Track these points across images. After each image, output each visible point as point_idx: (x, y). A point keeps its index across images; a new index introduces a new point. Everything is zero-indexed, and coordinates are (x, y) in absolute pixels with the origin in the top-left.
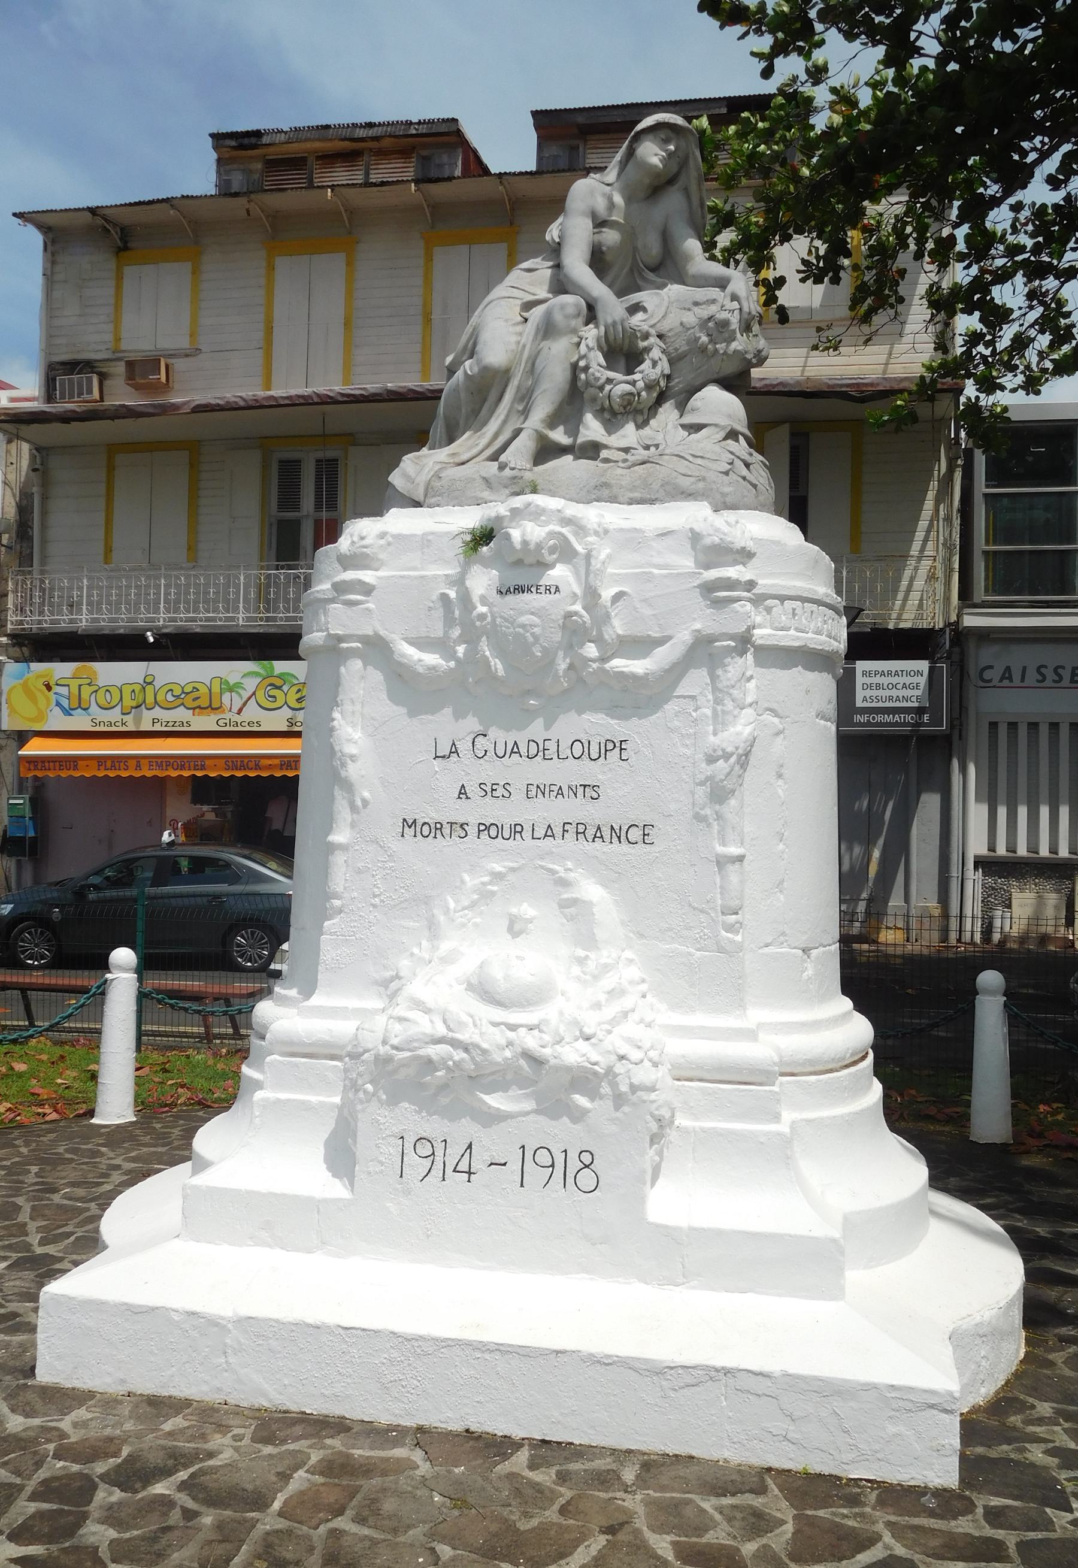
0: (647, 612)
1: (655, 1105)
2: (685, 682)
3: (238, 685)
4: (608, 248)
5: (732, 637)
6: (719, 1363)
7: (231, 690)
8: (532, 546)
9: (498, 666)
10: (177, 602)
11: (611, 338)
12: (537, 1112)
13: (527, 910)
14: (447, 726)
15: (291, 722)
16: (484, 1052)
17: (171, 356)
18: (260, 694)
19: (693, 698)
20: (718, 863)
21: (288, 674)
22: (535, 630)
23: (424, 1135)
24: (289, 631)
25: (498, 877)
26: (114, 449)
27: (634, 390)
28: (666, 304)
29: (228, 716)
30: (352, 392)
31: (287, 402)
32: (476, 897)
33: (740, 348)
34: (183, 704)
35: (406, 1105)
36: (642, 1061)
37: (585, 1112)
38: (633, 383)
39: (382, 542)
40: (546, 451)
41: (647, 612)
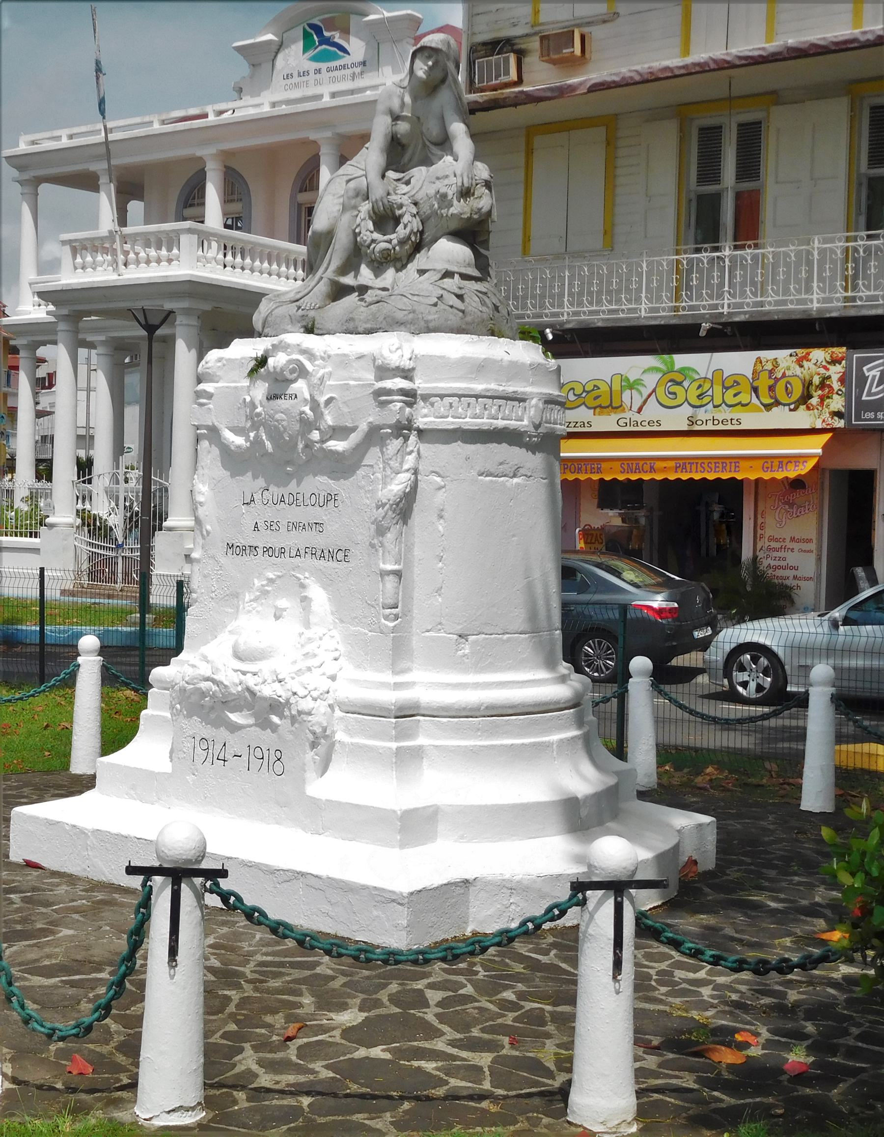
0: (346, 410)
1: (310, 724)
2: (368, 455)
3: (638, 382)
4: (402, 135)
5: (389, 427)
6: (298, 869)
7: (631, 388)
8: (278, 370)
9: (268, 445)
10: (581, 294)
11: (377, 211)
12: (255, 725)
13: (283, 603)
14: (250, 483)
15: (692, 421)
16: (226, 686)
17: (589, 24)
18: (660, 391)
19: (372, 466)
20: (381, 574)
21: (689, 369)
22: (284, 423)
23: (204, 736)
24: (690, 322)
25: (271, 581)
26: (532, 131)
27: (390, 246)
28: (423, 178)
29: (628, 415)
30: (750, 54)
31: (682, 71)
32: (258, 594)
33: (455, 212)
34: (584, 403)
35: (195, 718)
36: (306, 696)
37: (277, 726)
38: (390, 242)
39: (219, 364)
40: (339, 292)
41: (346, 410)
